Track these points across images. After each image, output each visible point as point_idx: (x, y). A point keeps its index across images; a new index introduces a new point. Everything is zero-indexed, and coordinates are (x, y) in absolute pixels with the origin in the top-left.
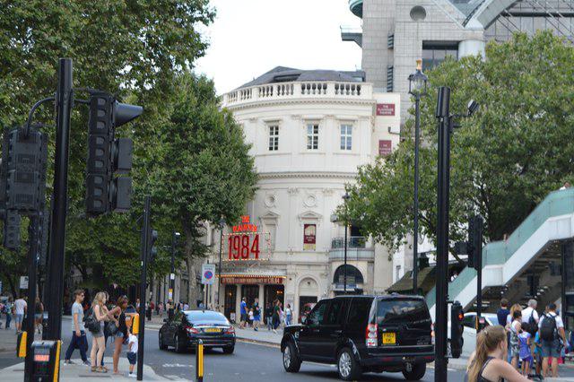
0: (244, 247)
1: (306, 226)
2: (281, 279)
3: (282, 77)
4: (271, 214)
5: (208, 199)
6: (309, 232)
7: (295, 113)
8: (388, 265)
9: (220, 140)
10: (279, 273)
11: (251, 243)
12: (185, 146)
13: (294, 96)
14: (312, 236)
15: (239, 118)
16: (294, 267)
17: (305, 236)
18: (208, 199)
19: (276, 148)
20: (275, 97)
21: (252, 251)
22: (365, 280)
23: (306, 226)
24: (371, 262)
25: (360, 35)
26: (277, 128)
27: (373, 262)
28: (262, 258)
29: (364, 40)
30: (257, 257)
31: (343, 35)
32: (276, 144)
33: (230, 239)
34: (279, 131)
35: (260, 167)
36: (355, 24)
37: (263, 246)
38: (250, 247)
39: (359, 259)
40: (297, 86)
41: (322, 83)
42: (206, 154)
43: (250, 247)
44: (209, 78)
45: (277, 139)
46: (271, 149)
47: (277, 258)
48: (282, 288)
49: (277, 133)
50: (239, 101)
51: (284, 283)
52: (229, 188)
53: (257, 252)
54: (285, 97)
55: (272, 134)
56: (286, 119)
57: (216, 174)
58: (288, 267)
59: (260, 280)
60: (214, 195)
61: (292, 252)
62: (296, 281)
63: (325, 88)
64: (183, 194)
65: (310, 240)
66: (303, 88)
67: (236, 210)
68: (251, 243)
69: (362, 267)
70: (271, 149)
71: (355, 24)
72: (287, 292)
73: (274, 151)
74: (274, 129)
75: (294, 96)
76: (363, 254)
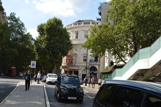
0: (70, 62)
1: (84, 57)
2: (78, 70)
3: (79, 22)
4: (76, 54)
5: (58, 49)
6: (85, 58)
7: (82, 29)
8: (10, 22)
9: (61, 34)
10: (77, 68)
11: (71, 60)
12: (53, 36)
13: (82, 25)
14: (85, 59)
15: (68, 31)
16: (81, 67)
17: (84, 59)
18: (58, 49)
19: (77, 38)
20: (77, 25)
21: (71, 63)
22: (98, 70)
23: (84, 57)
24: (99, 65)
25: (100, 19)
26: (78, 33)
27: (100, 65)
28: (73, 64)
29: (101, 20)
30: (72, 64)
31: (97, 19)
32: (77, 37)
33: (66, 60)
34: (78, 34)
35: (74, 42)
36: (100, 17)
37: (74, 61)
38: (71, 62)
39: (96, 65)
40: (83, 23)
41: (89, 22)
42: (57, 37)
43: (71, 62)
44: (60, 19)
45: (78, 36)
46: (76, 38)
47: (77, 64)
48: (78, 72)
49: (78, 34)
50: (69, 27)
51: (78, 71)
52: (63, 46)
53: (72, 63)
54: (80, 25)
55: (76, 35)
56: (80, 31)
57: (60, 42)
58: (79, 67)
59: (73, 70)
60: (59, 48)
61: (80, 63)
62: (81, 70)
63: (89, 23)
64: (52, 47)
65: (85, 60)
66: (84, 23)
67: (65, 52)
68: (71, 60)
69: (97, 67)
70: (76, 38)
71: (100, 17)
72: (79, 73)
73: (77, 39)
74: (77, 34)
75: (82, 25)
76: (97, 63)
